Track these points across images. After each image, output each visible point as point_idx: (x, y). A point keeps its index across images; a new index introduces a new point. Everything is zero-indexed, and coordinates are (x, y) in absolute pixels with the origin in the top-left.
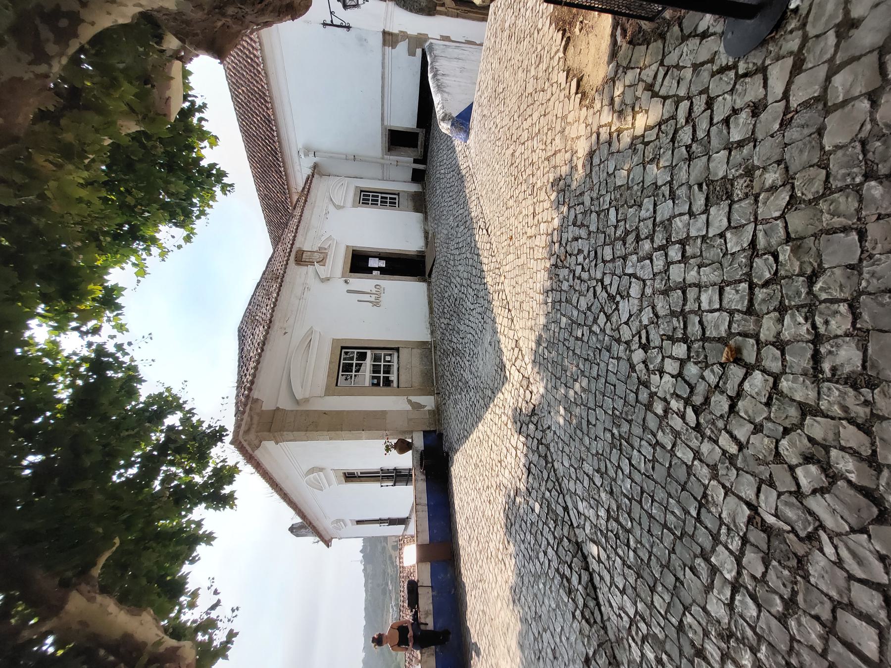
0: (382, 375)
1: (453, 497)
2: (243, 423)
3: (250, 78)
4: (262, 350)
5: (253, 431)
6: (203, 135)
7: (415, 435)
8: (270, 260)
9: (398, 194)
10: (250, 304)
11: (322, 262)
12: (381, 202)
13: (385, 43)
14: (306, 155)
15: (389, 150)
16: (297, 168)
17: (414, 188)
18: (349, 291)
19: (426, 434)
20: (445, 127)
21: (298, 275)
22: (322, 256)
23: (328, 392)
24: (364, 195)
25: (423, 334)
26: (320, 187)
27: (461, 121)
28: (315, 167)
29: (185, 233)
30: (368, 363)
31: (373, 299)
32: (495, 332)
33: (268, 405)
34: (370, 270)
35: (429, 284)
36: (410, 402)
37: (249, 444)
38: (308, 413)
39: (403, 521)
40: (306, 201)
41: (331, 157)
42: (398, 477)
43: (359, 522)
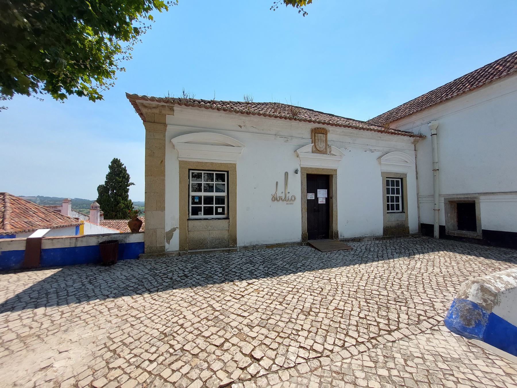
9: (403, 212)
12: (388, 197)
17: (413, 225)
18: (286, 174)
19: (141, 245)
24: (397, 182)
27: (484, 322)
28: (421, 137)
33: (169, 119)
35: (300, 244)
36: (174, 230)
40: (382, 132)
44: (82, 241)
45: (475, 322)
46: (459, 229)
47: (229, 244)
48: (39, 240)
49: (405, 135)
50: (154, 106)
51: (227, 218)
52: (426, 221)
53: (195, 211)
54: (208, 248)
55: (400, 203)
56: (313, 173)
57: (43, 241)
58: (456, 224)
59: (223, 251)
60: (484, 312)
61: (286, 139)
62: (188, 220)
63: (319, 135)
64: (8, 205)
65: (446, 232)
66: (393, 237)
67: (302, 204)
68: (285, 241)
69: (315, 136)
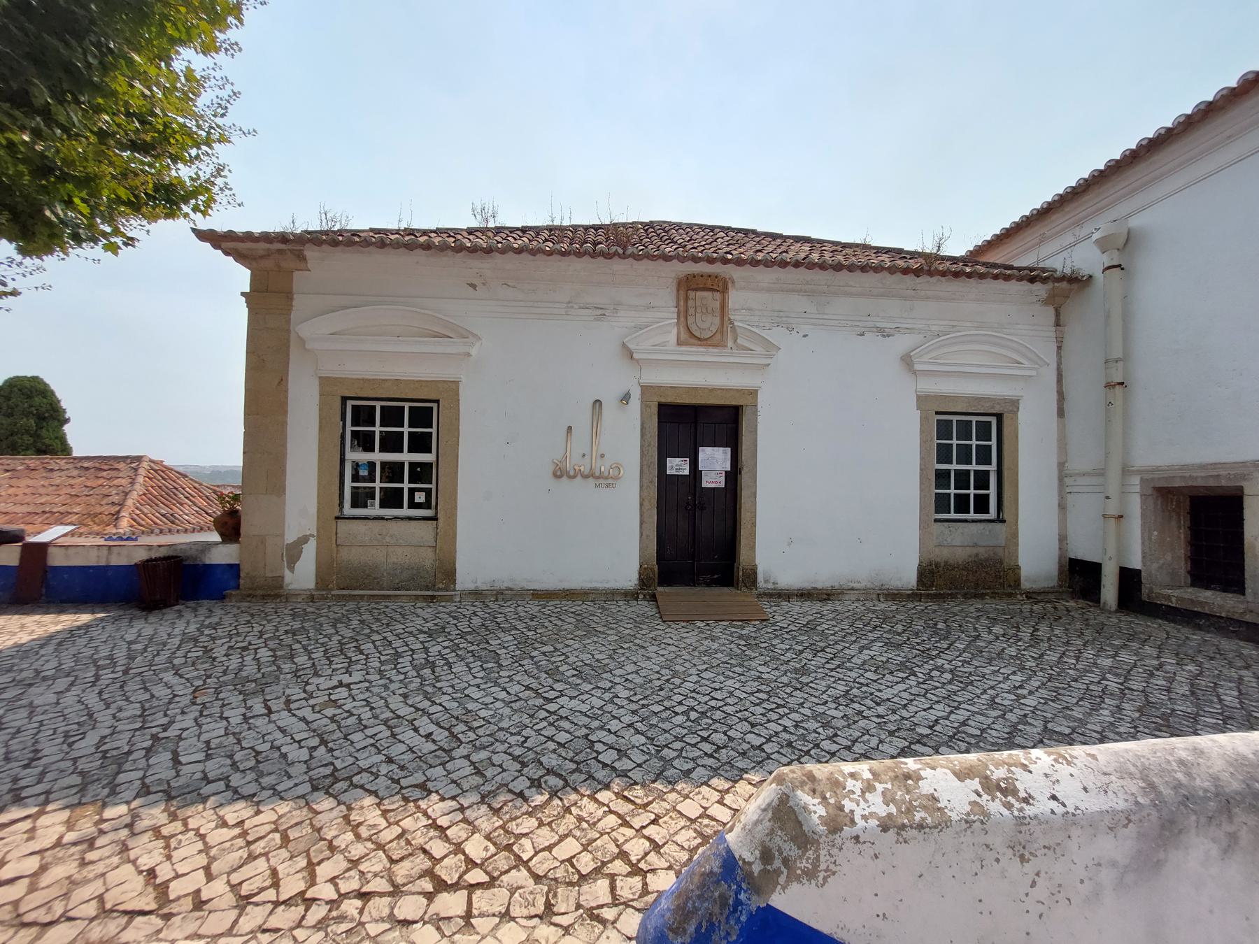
2: (249, 245)
9: (1000, 520)
17: (1036, 559)
19: (234, 569)
25: (472, 569)
28: (1077, 282)
36: (304, 540)
44: (119, 554)
45: (699, 926)
46: (1193, 585)
47: (435, 581)
48: (43, 547)
49: (1007, 278)
50: (261, 253)
51: (435, 519)
52: (1084, 551)
53: (360, 500)
54: (383, 589)
55: (992, 492)
56: (679, 401)
57: (51, 550)
58: (1182, 568)
59: (417, 597)
60: (742, 896)
61: (600, 312)
62: (337, 518)
63: (699, 293)
64: (140, 479)
65: (1145, 591)
66: (953, 596)
67: (641, 487)
69: (686, 299)
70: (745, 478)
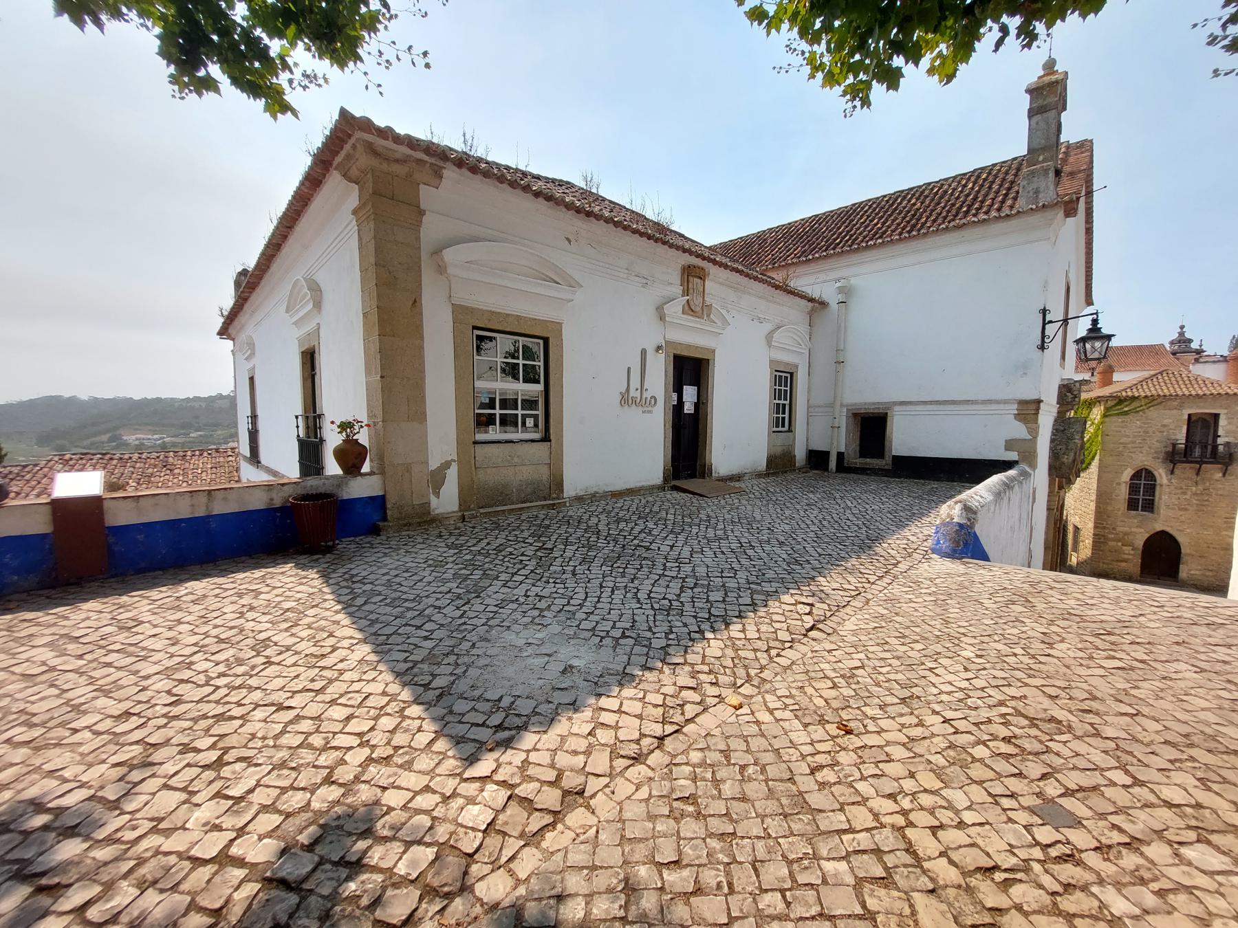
0: (520, 412)
1: (223, 573)
2: (389, 144)
3: (938, 210)
4: (537, 194)
5: (375, 162)
6: (964, 48)
7: (376, 479)
8: (683, 236)
10: (611, 202)
11: (689, 309)
12: (778, 405)
13: (1022, 403)
14: (841, 290)
15: (855, 415)
16: (822, 277)
17: (800, 454)
18: (644, 352)
19: (379, 502)
20: (950, 510)
21: (671, 264)
22: (698, 309)
23: (460, 312)
26: (794, 311)
28: (823, 304)
29: (771, 10)
30: (521, 389)
31: (633, 393)
32: (598, 687)
33: (427, 196)
34: (679, 390)
35: (661, 488)
36: (447, 465)
37: (348, 157)
38: (415, 269)
39: (254, 458)
41: (839, 327)
42: (310, 451)
43: (252, 379)
44: (225, 499)
47: (550, 490)
50: (398, 156)
59: (543, 506)
68: (639, 485)
70: (705, 404)
